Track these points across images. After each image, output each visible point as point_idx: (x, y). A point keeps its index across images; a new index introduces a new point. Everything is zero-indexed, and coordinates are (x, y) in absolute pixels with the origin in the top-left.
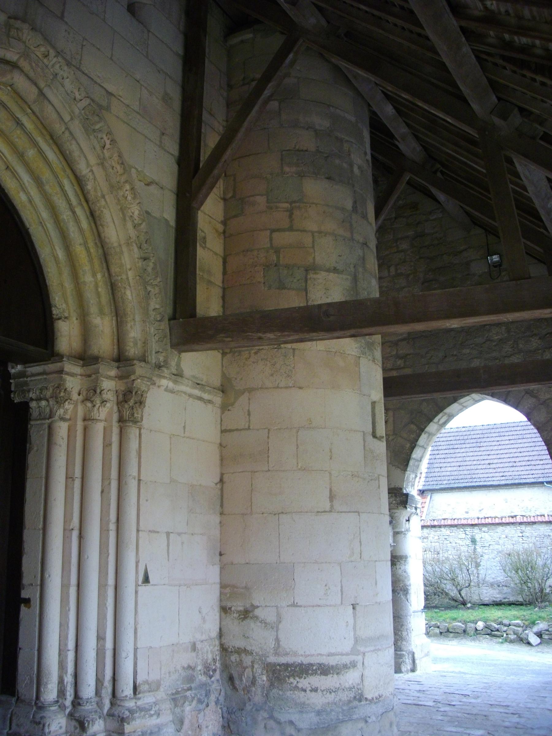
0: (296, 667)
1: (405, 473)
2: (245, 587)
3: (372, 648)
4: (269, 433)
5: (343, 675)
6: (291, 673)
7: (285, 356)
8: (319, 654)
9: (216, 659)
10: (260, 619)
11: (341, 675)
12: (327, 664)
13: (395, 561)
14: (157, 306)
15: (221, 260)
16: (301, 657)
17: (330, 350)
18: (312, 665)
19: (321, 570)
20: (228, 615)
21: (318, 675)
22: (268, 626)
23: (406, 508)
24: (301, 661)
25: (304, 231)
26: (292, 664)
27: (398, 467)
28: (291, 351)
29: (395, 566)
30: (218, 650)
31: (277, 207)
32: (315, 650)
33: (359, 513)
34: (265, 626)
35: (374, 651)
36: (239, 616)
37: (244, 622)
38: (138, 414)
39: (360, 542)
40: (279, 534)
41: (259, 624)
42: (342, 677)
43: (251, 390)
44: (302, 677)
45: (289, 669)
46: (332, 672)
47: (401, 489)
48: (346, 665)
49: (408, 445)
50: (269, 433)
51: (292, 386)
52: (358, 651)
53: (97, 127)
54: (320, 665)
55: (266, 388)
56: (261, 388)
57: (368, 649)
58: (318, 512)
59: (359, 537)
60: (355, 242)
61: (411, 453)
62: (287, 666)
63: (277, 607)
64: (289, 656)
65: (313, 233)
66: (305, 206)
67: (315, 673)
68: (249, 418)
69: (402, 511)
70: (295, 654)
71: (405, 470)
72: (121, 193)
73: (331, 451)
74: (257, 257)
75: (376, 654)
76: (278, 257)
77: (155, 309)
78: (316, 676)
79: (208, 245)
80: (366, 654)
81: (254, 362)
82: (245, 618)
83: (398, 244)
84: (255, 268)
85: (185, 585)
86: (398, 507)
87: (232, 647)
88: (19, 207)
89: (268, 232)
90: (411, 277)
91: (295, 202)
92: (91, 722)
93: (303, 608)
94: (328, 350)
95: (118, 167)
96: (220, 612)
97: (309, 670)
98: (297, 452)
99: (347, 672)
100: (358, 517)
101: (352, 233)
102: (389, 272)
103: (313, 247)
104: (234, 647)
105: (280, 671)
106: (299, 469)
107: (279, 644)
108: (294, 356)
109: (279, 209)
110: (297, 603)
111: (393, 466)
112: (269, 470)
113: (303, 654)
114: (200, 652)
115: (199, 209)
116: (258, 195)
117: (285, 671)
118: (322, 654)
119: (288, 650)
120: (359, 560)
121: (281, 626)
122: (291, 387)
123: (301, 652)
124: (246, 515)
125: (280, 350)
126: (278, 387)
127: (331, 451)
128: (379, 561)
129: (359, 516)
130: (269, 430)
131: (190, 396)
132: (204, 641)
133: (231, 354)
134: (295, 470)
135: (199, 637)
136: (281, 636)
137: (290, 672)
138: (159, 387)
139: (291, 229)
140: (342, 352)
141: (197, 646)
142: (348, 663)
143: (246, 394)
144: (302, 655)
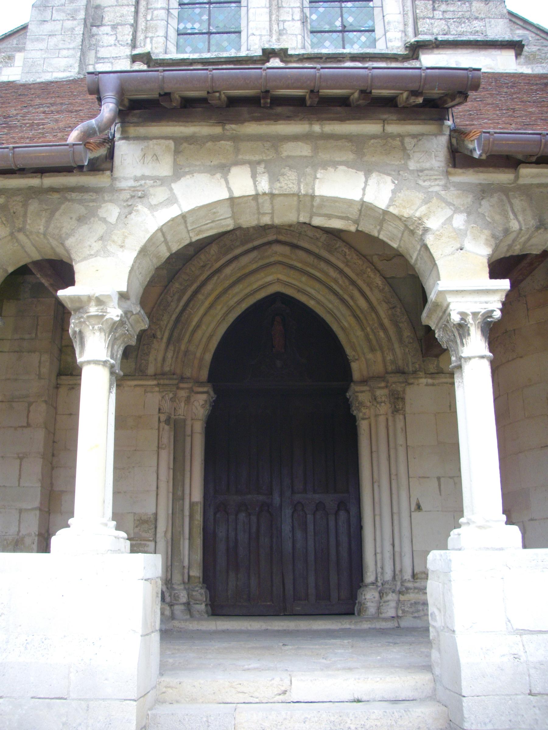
14: (409, 334)
38: (399, 405)
53: (337, 246)
58: (542, 447)
72: (365, 276)
77: (408, 337)
88: (313, 308)
92: (385, 594)
94: (539, 322)
95: (359, 261)
138: (418, 384)
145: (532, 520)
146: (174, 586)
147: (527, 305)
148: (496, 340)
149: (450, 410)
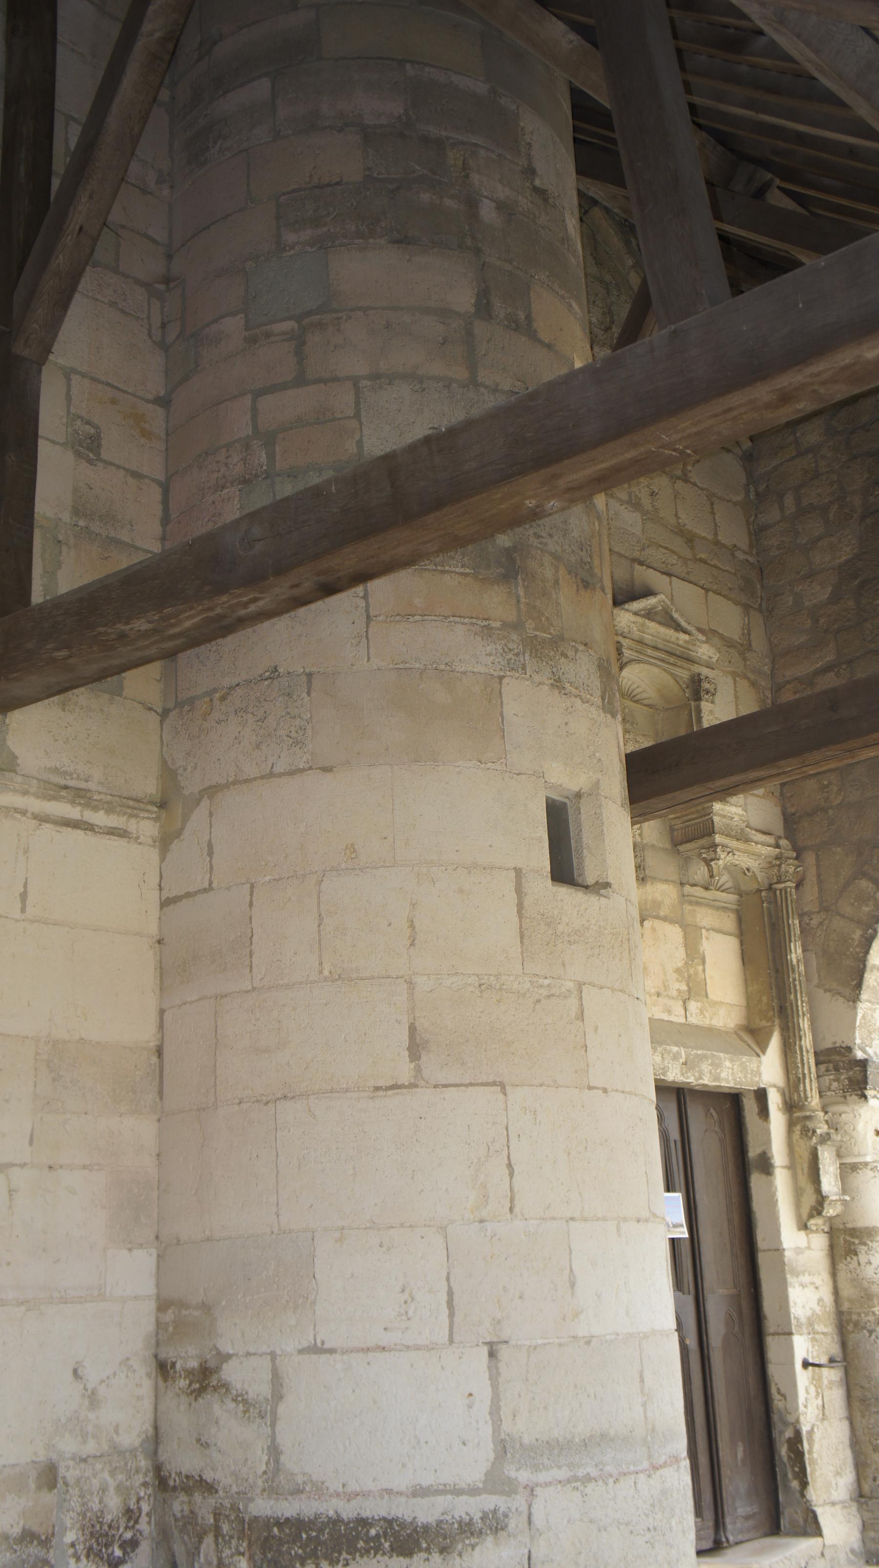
0: (321, 1531)
1: (855, 1008)
2: (203, 1302)
3: (563, 1474)
4: (252, 894)
5: (460, 1555)
6: (308, 1550)
7: (289, 695)
8: (386, 1490)
9: (140, 1509)
10: (234, 1392)
11: (455, 1555)
12: (409, 1520)
13: (854, 1243)
15: (156, 493)
16: (334, 1501)
17: (407, 665)
18: (364, 1522)
19: (389, 1249)
20: (170, 1382)
21: (384, 1554)
22: (251, 1410)
23: (865, 1097)
24: (336, 1512)
25: (335, 379)
26: (310, 1521)
27: (839, 994)
28: (304, 678)
29: (855, 1258)
30: (145, 1484)
31: (268, 335)
32: (374, 1480)
33: (502, 1086)
34: (245, 1412)
35: (569, 1481)
36: (190, 1384)
37: (200, 1400)
39: (510, 1166)
40: (277, 1155)
41: (232, 1405)
42: (458, 1560)
43: (212, 791)
44: (338, 1562)
45: (304, 1536)
46: (424, 1545)
47: (849, 1049)
48: (470, 1523)
49: (857, 934)
50: (252, 894)
51: (307, 766)
52: (510, 1481)
54: (389, 1522)
55: (246, 781)
56: (234, 783)
57: (543, 1477)
58: (377, 1089)
59: (505, 1153)
60: (482, 390)
61: (867, 952)
62: (297, 1525)
63: (273, 1356)
64: (303, 1496)
65: (355, 381)
66: (337, 318)
67: (374, 1548)
68: (211, 861)
69: (856, 1108)
70: (319, 1490)
71: (855, 999)
73: (412, 926)
74: (226, 464)
75: (578, 1494)
76: (271, 457)
78: (379, 1557)
79: (105, 455)
80: (538, 1491)
81: (219, 722)
82: (202, 1390)
83: (798, 435)
84: (222, 491)
85: (22, 1303)
86: (845, 1097)
87: (176, 1473)
89: (248, 400)
90: (834, 508)
91: (310, 313)
93: (337, 1356)
96: (156, 1377)
97: (357, 1538)
98: (320, 935)
99: (473, 1547)
100: (501, 1096)
101: (473, 369)
102: (782, 508)
103: (357, 416)
104: (179, 1474)
105: (281, 1542)
106: (326, 979)
107: (277, 1461)
108: (309, 694)
109: (272, 339)
110: (323, 1343)
111: (825, 991)
112: (254, 989)
113: (340, 1490)
114: (74, 1492)
115: (42, 360)
116: (226, 315)
117: (294, 1542)
118: (395, 1490)
119: (300, 1479)
120: (508, 1216)
121: (281, 1409)
122: (303, 770)
123: (334, 1485)
124: (204, 1109)
125: (276, 682)
126: (272, 775)
127: (412, 926)
128: (585, 1220)
129: (505, 1094)
130: (252, 887)
131: (42, 819)
132: (90, 1460)
133: (177, 710)
134: (315, 982)
135: (68, 1445)
136: (285, 1440)
137: (307, 1545)
139: (301, 380)
140: (442, 667)
141: (62, 1471)
142: (477, 1517)
143: (205, 803)
144: (338, 1495)
145: (316, 1349)
146: (126, 817)
147: (367, 603)
148: (223, 698)
149: (23, 910)
